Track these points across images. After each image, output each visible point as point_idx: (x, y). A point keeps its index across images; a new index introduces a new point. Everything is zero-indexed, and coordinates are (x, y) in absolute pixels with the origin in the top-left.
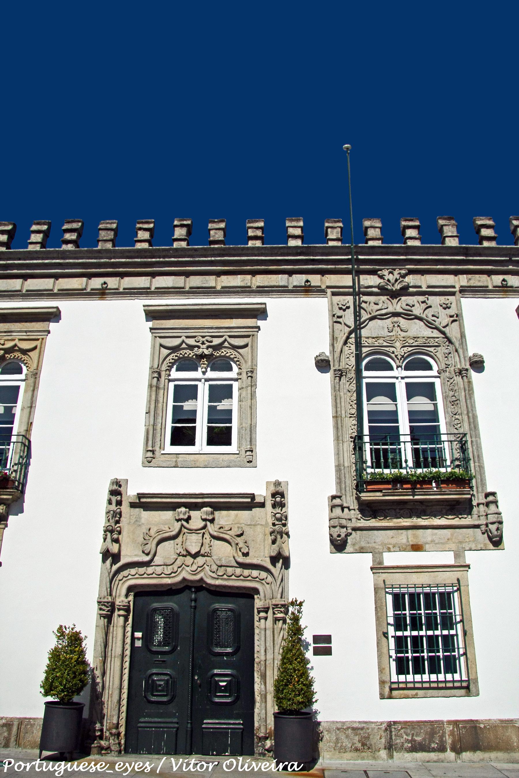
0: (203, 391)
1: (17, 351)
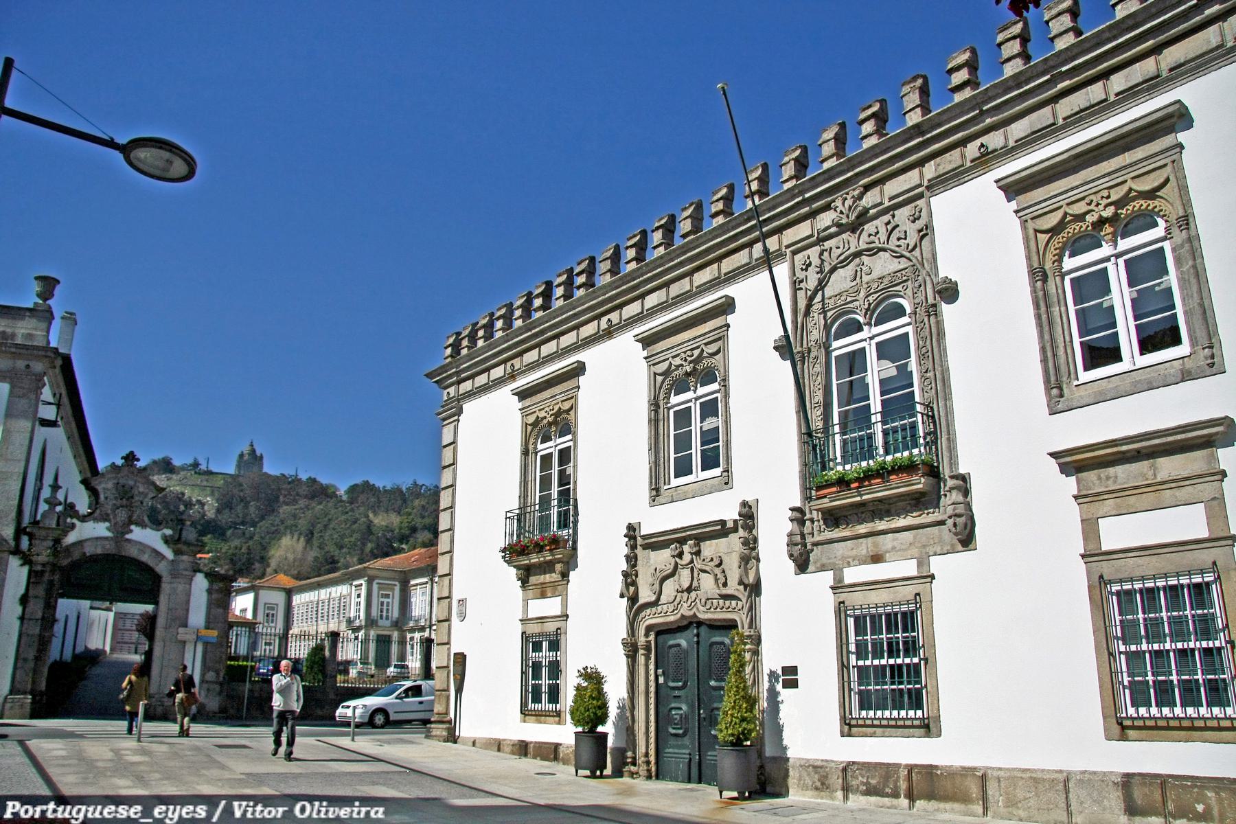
0: (1117, 276)
1: (1134, 199)
